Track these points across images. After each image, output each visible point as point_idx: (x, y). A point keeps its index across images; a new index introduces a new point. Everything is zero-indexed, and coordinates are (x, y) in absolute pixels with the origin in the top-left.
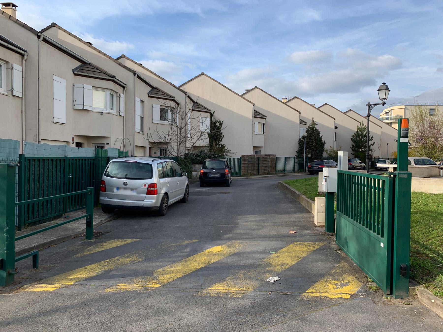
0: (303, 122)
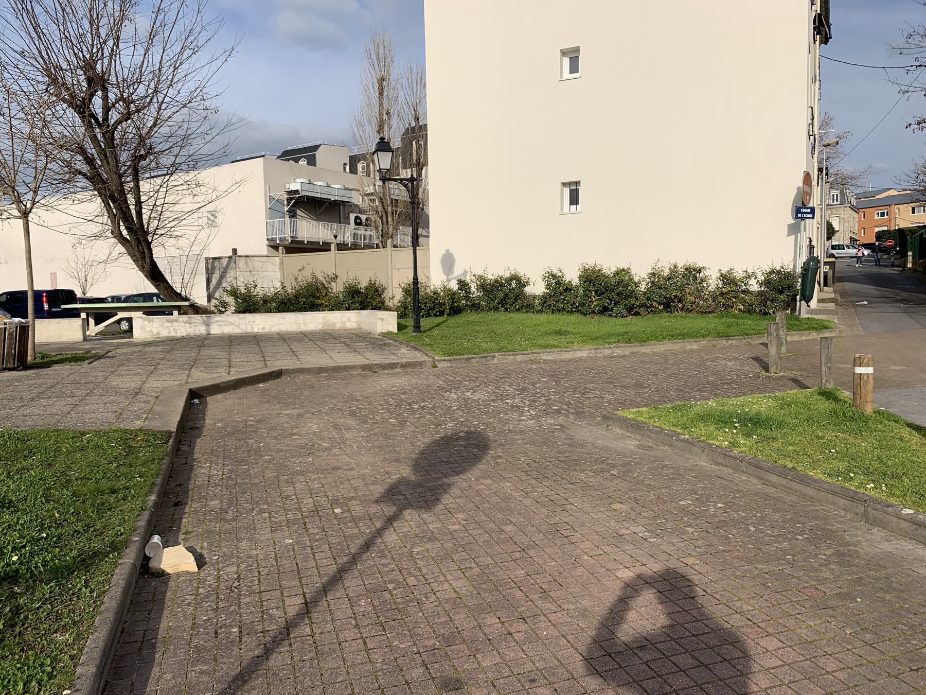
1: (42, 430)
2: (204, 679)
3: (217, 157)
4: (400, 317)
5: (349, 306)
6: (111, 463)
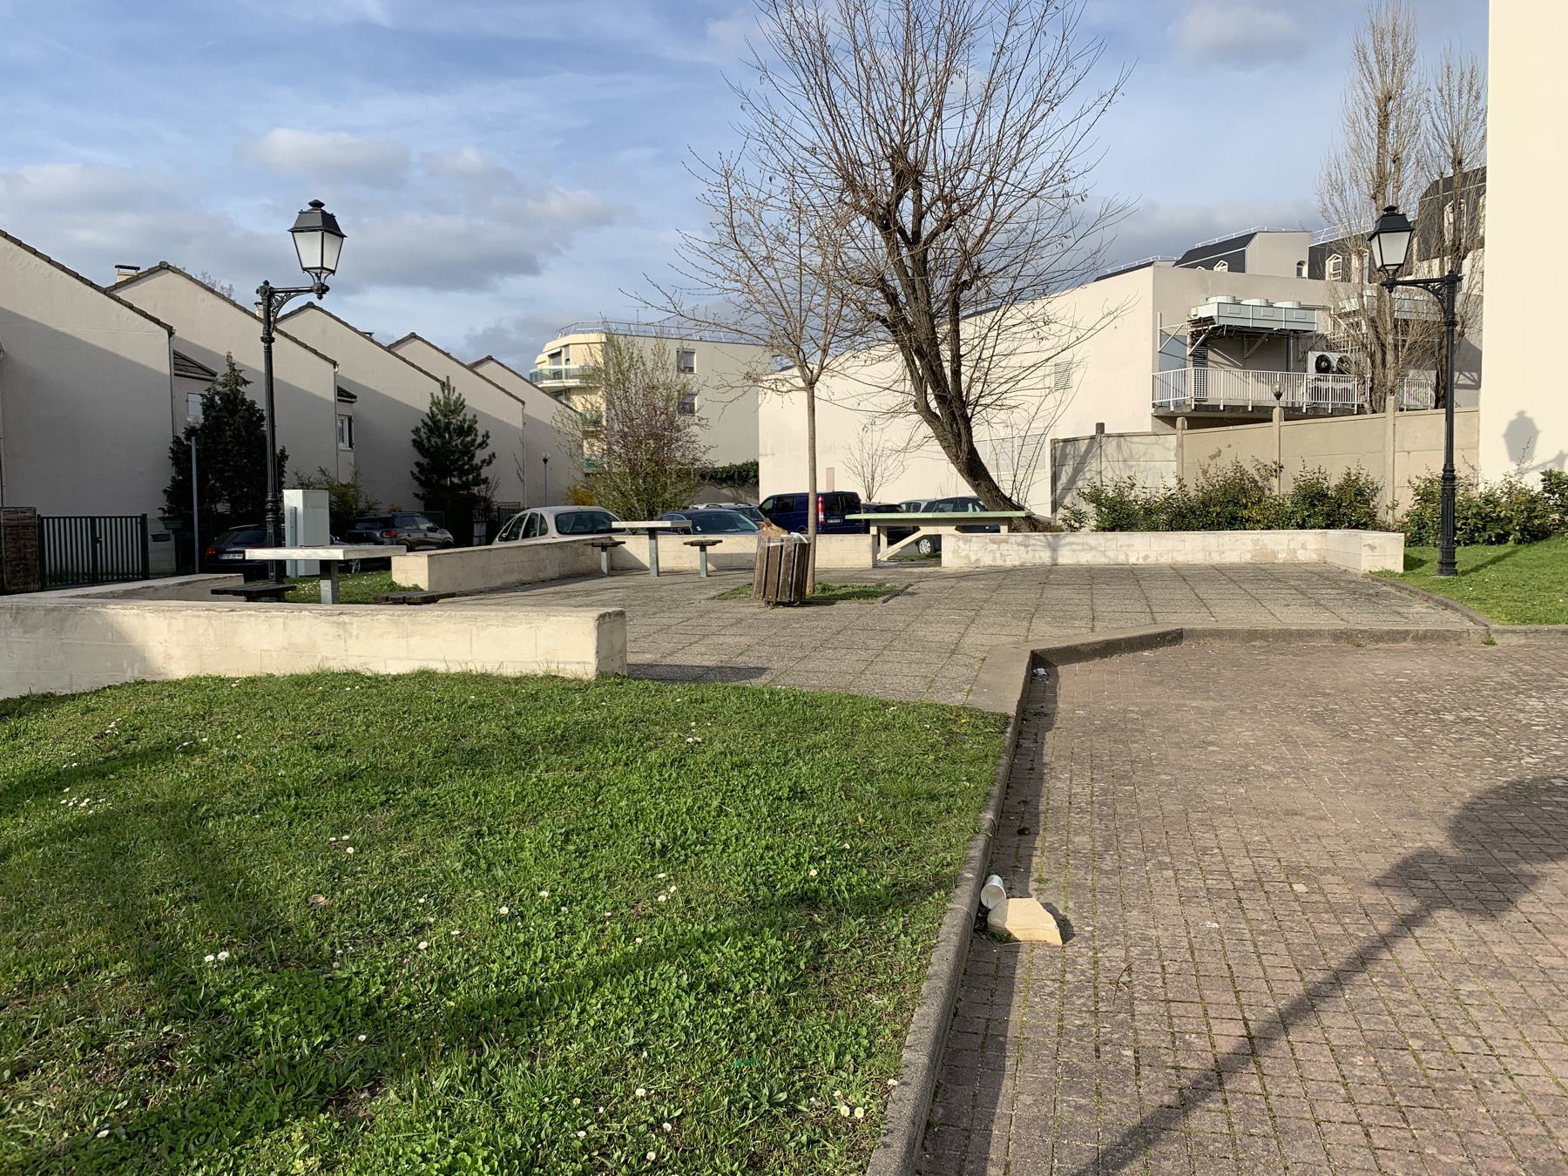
0: (183, 365)
1: (833, 694)
2: (1082, 1118)
3: (1079, 273)
4: (1409, 543)
5: (1304, 520)
6: (925, 753)
